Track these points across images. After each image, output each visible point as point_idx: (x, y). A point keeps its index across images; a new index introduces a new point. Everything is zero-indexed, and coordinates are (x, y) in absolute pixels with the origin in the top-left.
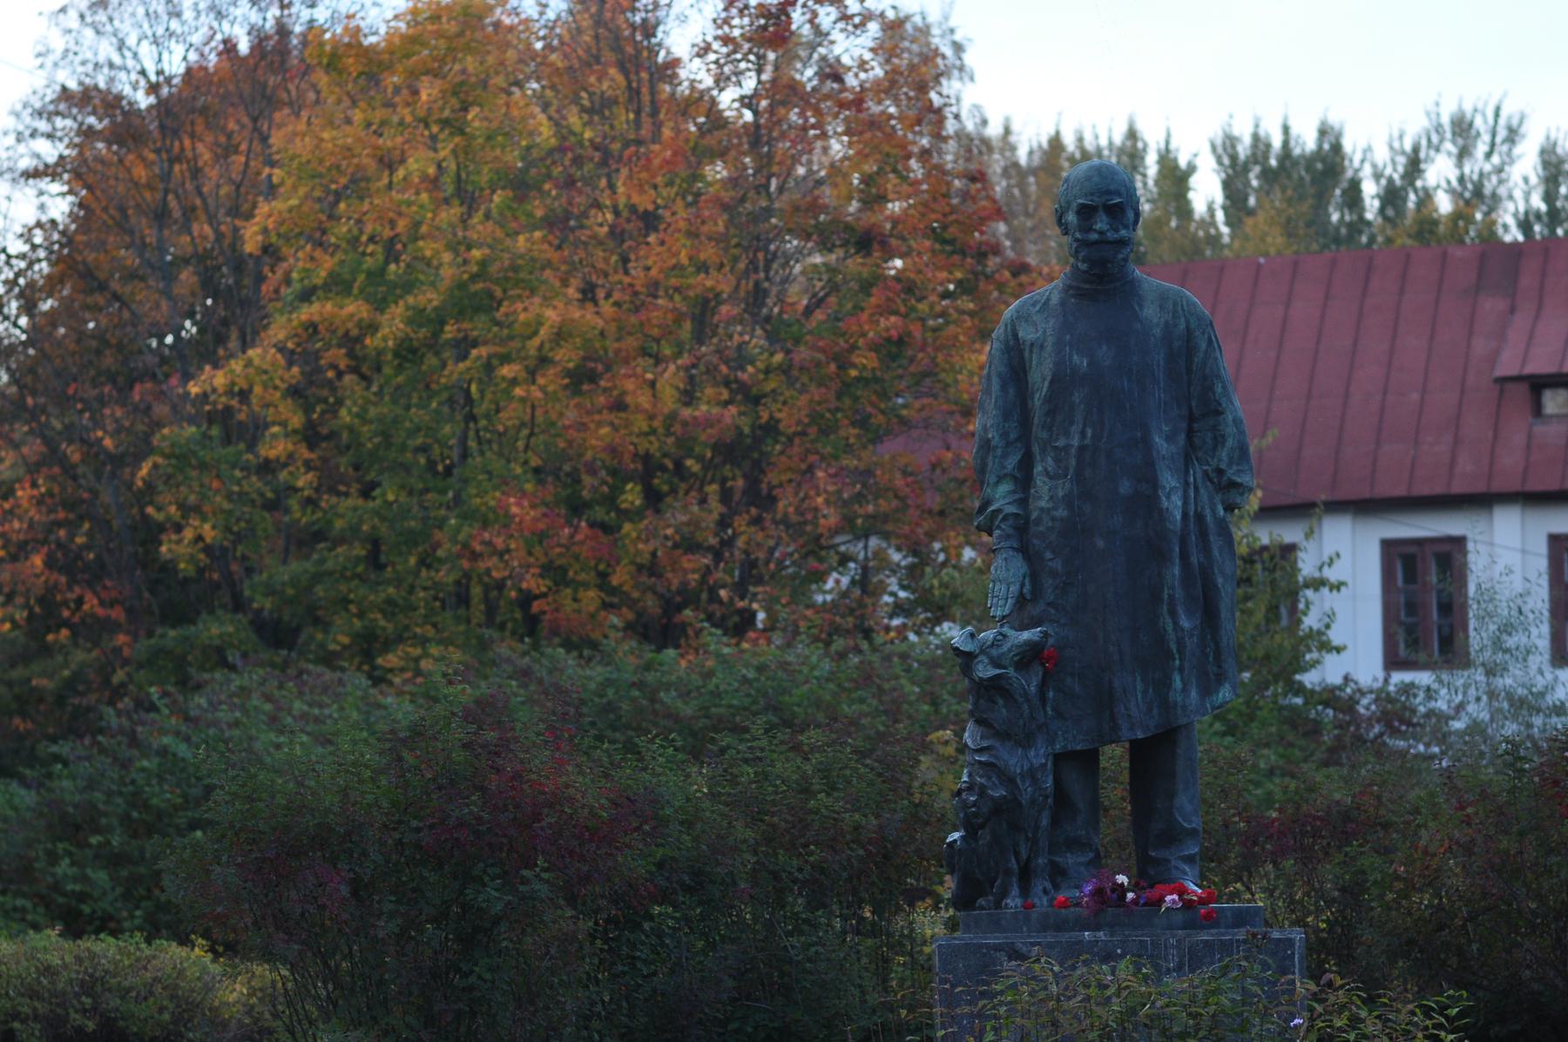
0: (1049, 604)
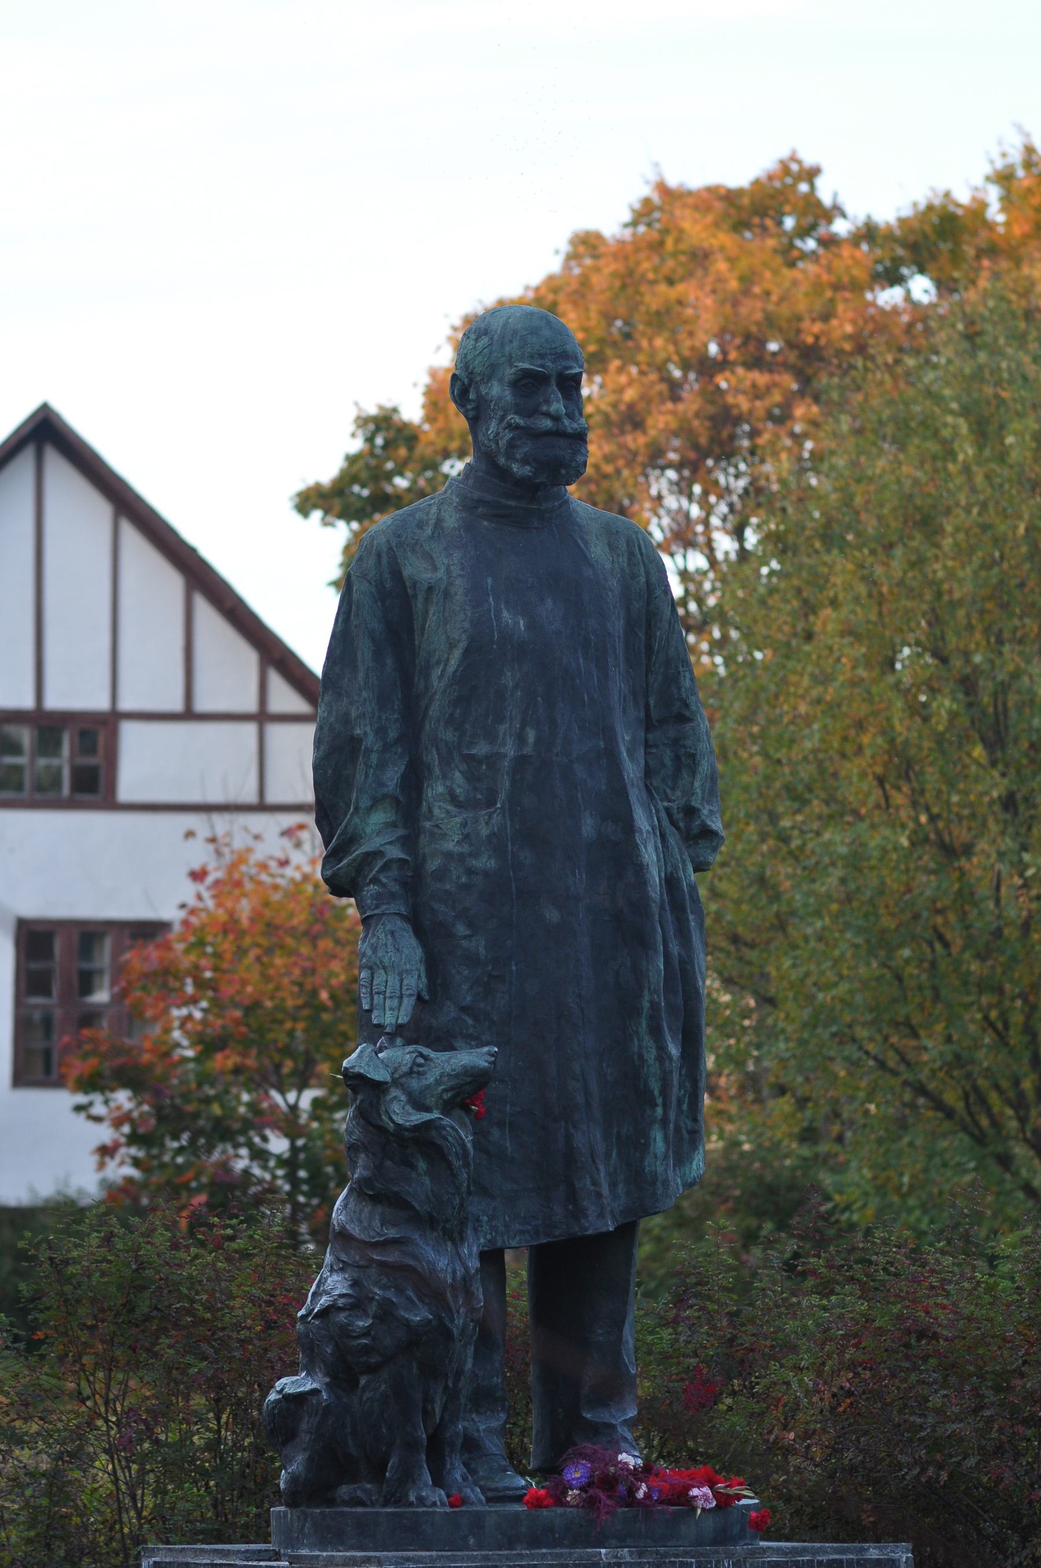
0: (464, 1009)
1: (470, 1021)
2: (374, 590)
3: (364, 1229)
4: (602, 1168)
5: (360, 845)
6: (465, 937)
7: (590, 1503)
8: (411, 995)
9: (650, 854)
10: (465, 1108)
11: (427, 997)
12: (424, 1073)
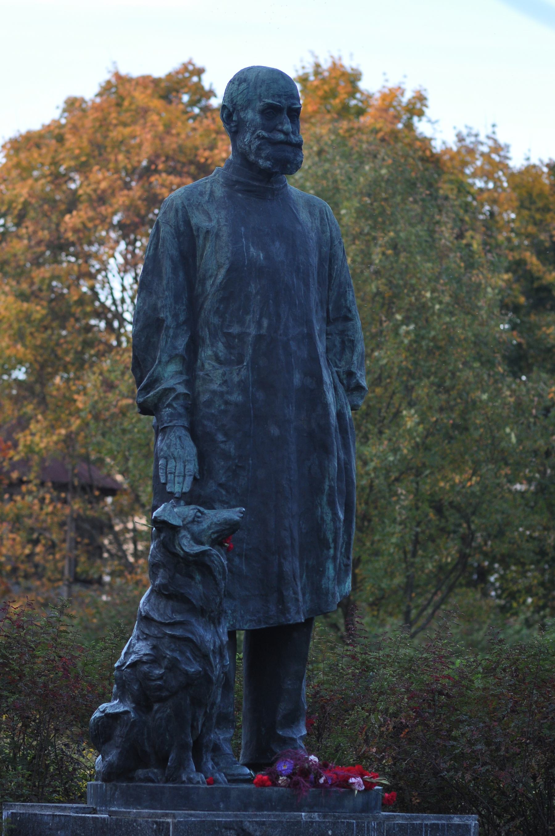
0: (220, 485)
1: (224, 493)
2: (173, 231)
3: (160, 615)
4: (299, 583)
5: (161, 384)
6: (223, 442)
7: (293, 785)
8: (190, 475)
9: (330, 397)
10: (221, 544)
11: (198, 477)
12: (201, 522)
